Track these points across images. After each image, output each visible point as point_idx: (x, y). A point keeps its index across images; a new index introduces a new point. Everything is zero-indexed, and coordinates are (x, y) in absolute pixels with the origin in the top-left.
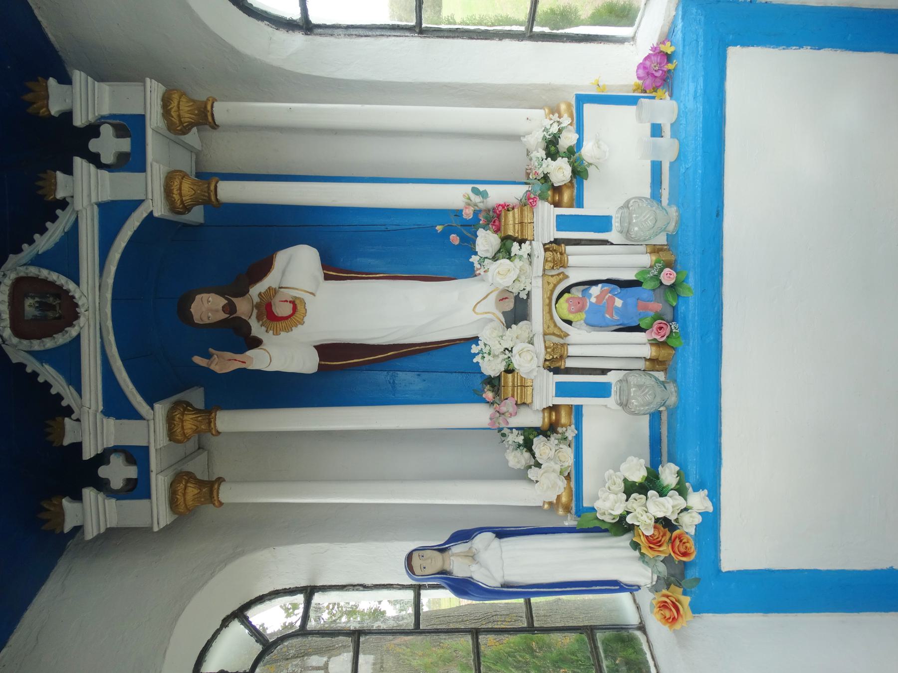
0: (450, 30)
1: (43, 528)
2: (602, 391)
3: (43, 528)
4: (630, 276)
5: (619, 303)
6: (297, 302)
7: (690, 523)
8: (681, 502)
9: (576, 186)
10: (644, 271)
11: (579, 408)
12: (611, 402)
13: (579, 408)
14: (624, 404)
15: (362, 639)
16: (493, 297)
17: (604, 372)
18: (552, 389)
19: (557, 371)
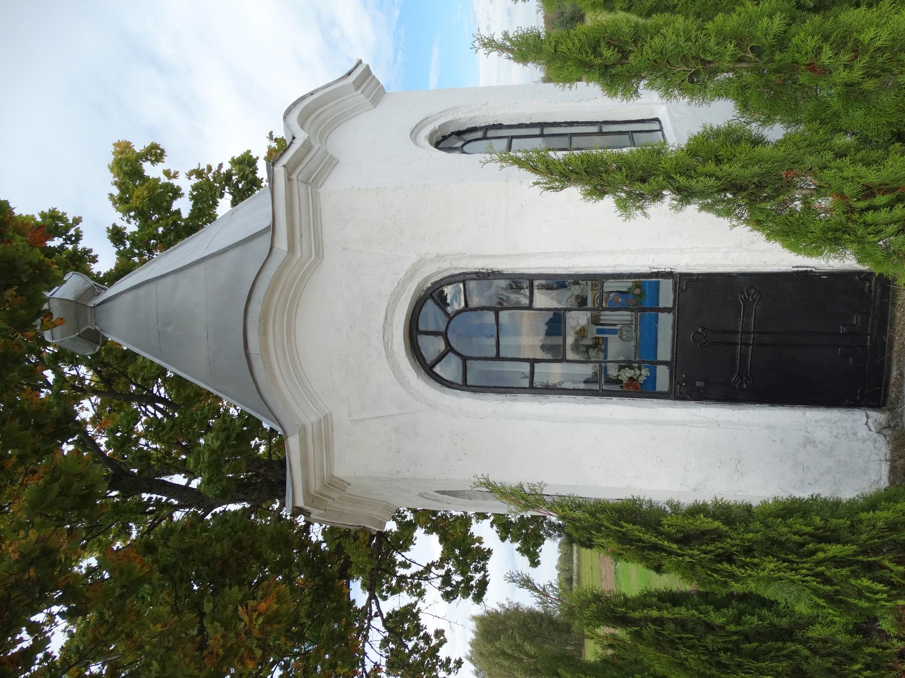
0: (574, 389)
1: (33, 619)
2: (614, 332)
3: (33, 619)
4: (625, 290)
5: (620, 300)
6: (434, 141)
7: (642, 379)
8: (638, 372)
9: (613, 527)
10: (630, 289)
11: (607, 338)
12: (617, 336)
13: (607, 338)
14: (621, 337)
15: (450, 353)
16: (574, 297)
17: (616, 325)
18: (595, 332)
19: (597, 325)
